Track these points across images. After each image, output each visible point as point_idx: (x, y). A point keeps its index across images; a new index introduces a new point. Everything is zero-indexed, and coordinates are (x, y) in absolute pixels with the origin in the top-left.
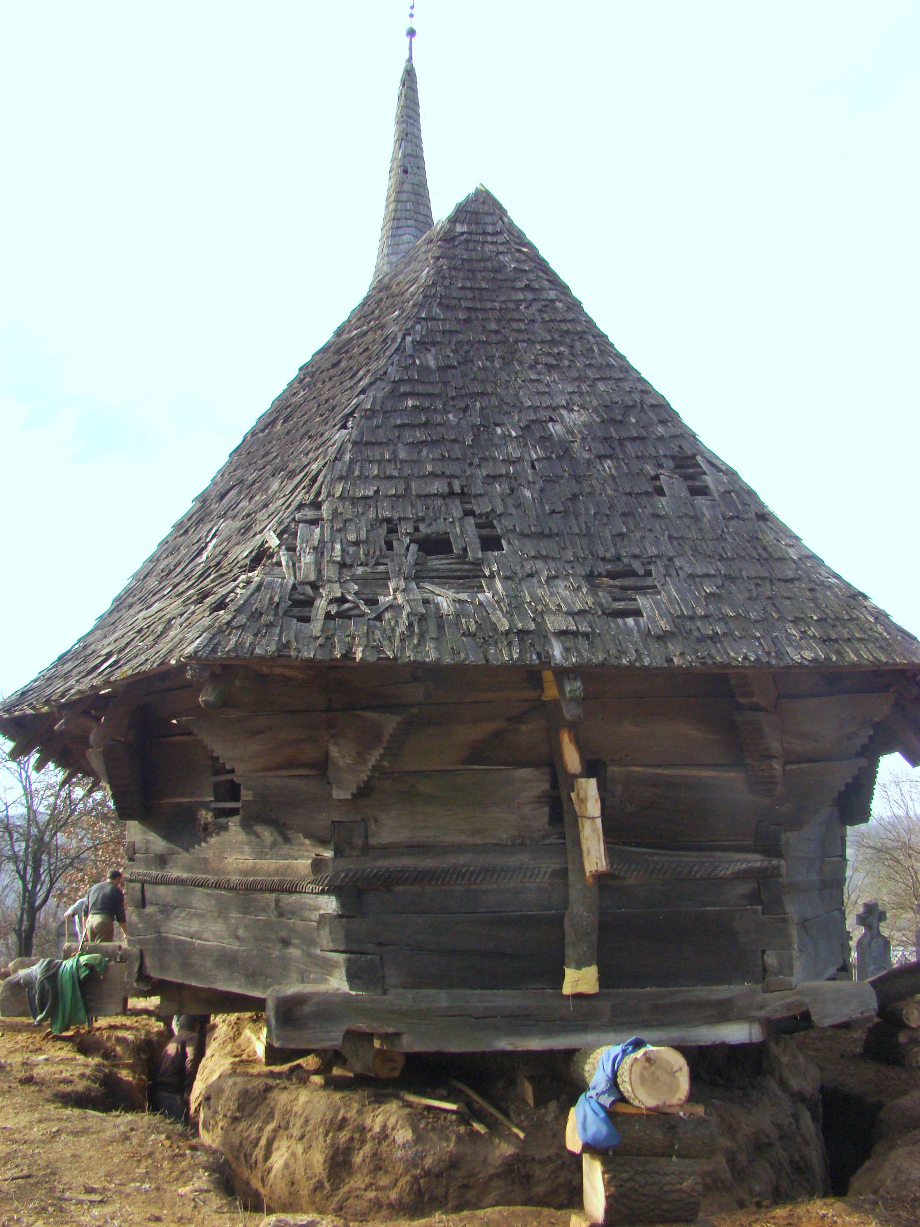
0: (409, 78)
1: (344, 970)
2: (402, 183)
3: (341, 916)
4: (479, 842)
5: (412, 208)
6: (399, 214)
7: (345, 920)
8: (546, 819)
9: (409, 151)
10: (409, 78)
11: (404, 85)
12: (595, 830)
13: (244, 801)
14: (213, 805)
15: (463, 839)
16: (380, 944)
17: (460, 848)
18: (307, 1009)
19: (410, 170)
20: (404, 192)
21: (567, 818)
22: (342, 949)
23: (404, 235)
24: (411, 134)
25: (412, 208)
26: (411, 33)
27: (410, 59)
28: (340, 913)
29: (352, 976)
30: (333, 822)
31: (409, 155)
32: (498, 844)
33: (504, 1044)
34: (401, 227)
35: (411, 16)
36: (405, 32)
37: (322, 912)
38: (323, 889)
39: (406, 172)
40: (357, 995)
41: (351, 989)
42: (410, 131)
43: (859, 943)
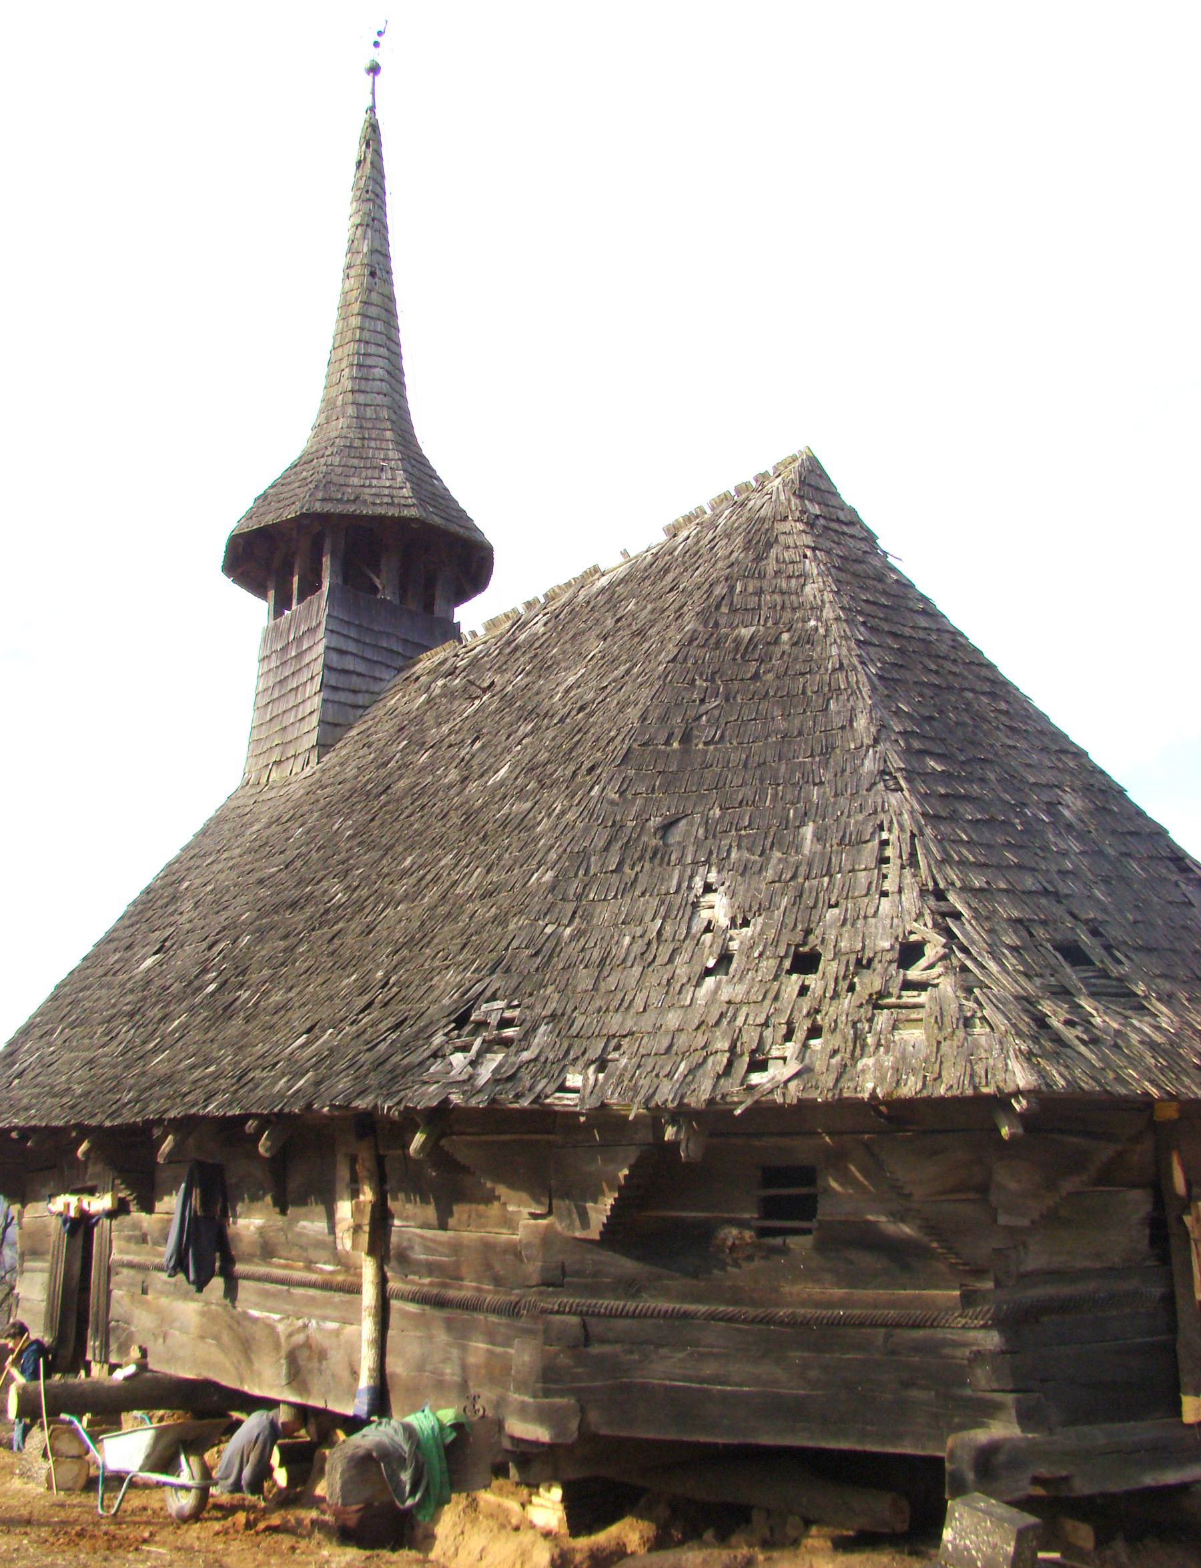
0: (372, 137)
1: (1013, 1412)
2: (369, 291)
3: (1003, 1352)
4: (1098, 1267)
5: (383, 330)
6: (367, 335)
7: (1008, 1356)
8: (1146, 1242)
9: (377, 246)
10: (372, 137)
11: (368, 146)
12: (357, 1211)
13: (819, 1221)
14: (753, 1223)
15: (1087, 1263)
16: (1042, 1380)
17: (1085, 1274)
18: (1001, 1458)
19: (378, 272)
20: (372, 304)
21: (1174, 1242)
22: (1010, 1387)
23: (375, 367)
24: (379, 221)
25: (383, 330)
26: (374, 70)
27: (372, 109)
28: (1004, 1348)
29: (1026, 1418)
30: (994, 1249)
31: (377, 250)
32: (1110, 1269)
33: (1149, 1480)
34: (370, 355)
35: (376, 44)
36: (382, 71)
37: (975, 1348)
38: (986, 1323)
39: (373, 274)
40: (1034, 1438)
41: (1023, 1431)
42: (377, 216)
43: (506, 1353)
